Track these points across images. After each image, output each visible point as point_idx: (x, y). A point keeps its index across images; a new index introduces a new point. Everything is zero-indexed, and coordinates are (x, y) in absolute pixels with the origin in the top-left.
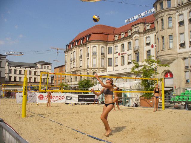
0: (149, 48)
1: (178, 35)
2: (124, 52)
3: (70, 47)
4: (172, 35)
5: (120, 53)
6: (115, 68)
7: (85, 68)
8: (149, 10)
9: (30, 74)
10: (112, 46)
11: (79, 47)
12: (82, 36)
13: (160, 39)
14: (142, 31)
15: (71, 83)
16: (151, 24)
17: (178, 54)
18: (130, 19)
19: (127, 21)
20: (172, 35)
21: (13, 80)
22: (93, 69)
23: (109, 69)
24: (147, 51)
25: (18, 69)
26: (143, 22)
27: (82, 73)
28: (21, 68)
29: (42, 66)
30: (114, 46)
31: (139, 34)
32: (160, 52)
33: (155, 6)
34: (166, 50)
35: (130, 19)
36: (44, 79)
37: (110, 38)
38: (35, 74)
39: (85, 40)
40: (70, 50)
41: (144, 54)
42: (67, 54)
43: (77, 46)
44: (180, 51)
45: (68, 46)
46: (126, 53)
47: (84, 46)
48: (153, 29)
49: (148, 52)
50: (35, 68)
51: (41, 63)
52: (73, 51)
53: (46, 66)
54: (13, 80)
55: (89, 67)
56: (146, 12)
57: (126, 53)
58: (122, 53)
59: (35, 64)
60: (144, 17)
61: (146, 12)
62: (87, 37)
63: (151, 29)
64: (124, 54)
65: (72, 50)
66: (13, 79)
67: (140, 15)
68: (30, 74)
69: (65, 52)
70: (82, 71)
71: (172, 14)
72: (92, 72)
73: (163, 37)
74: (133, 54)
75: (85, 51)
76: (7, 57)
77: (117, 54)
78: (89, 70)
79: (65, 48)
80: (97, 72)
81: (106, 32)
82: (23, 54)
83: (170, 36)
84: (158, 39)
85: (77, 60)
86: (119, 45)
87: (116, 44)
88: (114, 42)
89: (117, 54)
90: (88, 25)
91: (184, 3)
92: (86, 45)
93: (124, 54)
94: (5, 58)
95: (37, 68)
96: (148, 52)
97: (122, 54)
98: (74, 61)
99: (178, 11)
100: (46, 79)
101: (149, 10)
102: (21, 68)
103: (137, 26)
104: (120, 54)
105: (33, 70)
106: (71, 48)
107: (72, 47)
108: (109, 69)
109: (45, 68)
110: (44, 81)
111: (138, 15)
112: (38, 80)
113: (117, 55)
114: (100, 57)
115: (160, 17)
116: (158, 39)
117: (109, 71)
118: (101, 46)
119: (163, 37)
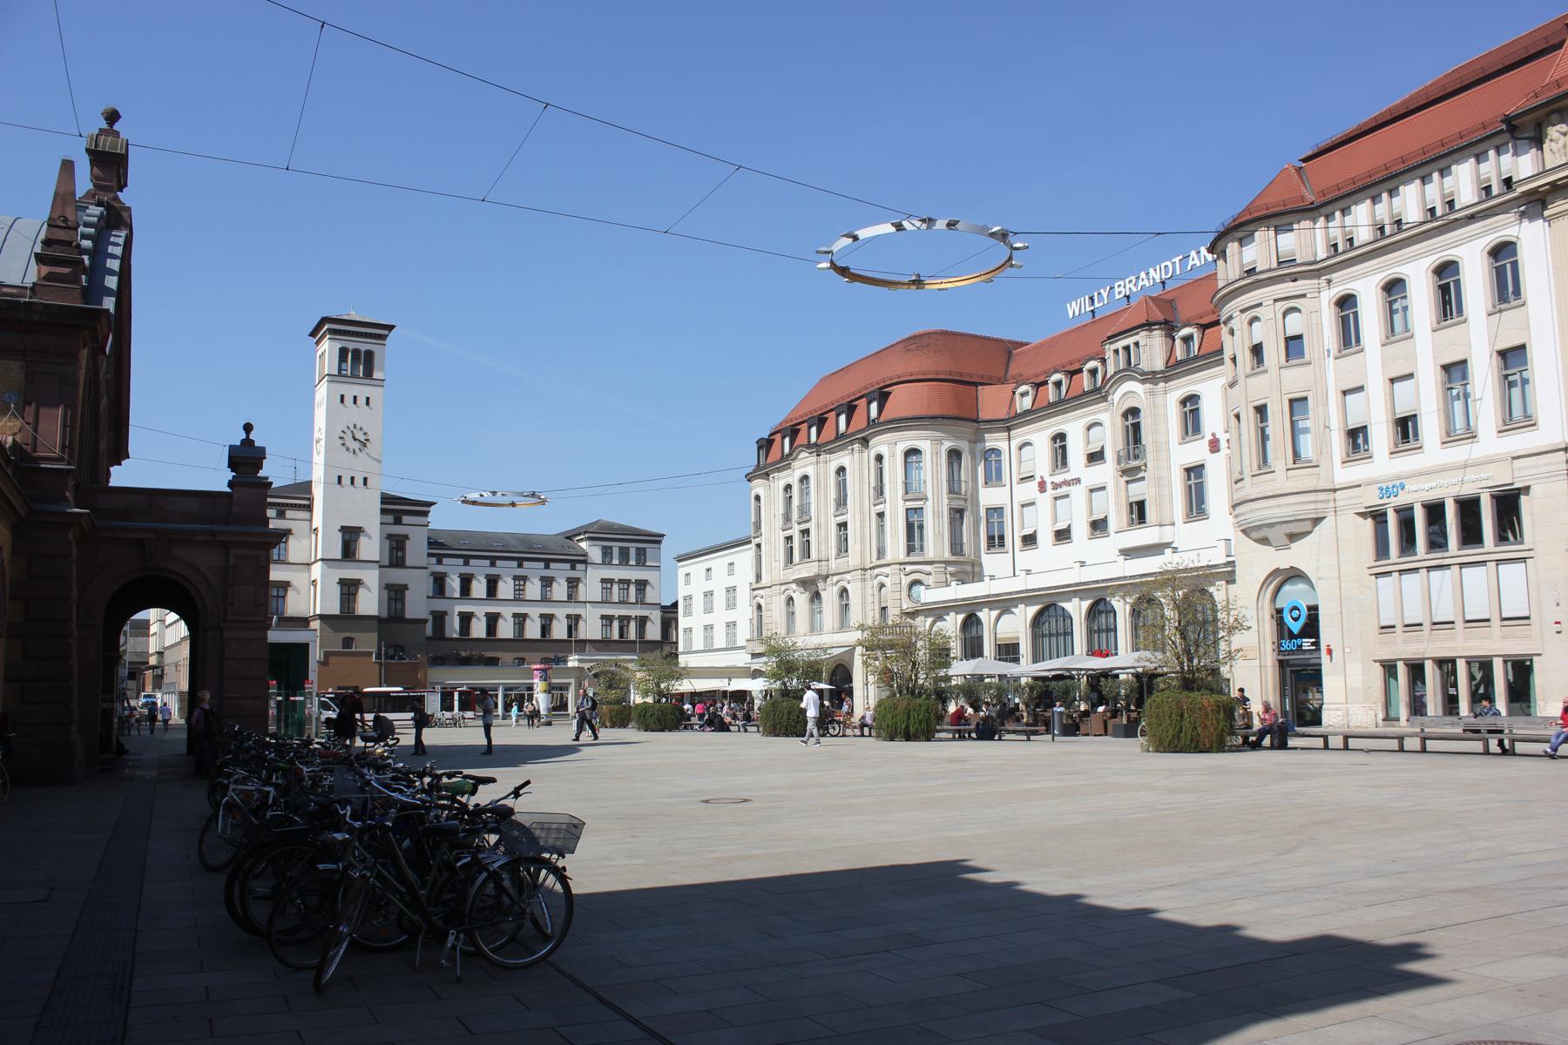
0: (1196, 451)
1: (1334, 398)
2: (1068, 476)
3: (770, 453)
4: (1305, 399)
5: (1048, 480)
6: (1026, 558)
7: (868, 565)
8: (1193, 253)
9: (519, 598)
10: (1002, 445)
11: (831, 452)
12: (842, 392)
13: (1249, 417)
14: (1159, 365)
15: (814, 641)
16: (1204, 327)
17: (1335, 490)
18: (1092, 299)
19: (1076, 308)
20: (1305, 399)
21: (538, 636)
22: (909, 568)
23: (992, 562)
24: (1188, 470)
25: (480, 570)
26: (1162, 318)
27: (849, 587)
28: (466, 563)
29: (607, 553)
30: (1015, 443)
31: (1143, 382)
32: (1248, 479)
33: (1219, 248)
34: (1280, 473)
35: (1092, 299)
36: (624, 620)
37: (991, 400)
38: (571, 597)
39: (859, 416)
40: (779, 470)
41: (1170, 485)
42: (761, 491)
43: (817, 449)
44: (1344, 475)
45: (766, 445)
46: (1078, 481)
47: (856, 446)
48: (1213, 357)
49: (1195, 472)
50: (573, 564)
51: (604, 533)
52: (798, 474)
53: (633, 547)
54: (538, 636)
55: (889, 558)
56: (1176, 260)
57: (1078, 481)
58: (1058, 479)
59: (569, 537)
60: (1168, 288)
61: (1176, 260)
62: (869, 403)
63: (1204, 357)
64: (1067, 483)
65: (788, 467)
66: (478, 630)
67: (1143, 275)
68: (709, 609)
69: (750, 478)
70: (848, 577)
71: (1304, 296)
72: (906, 581)
73: (1261, 410)
74: (1116, 485)
75: (861, 476)
76: (432, 508)
77: (1034, 485)
78: (886, 570)
79: (751, 458)
80: (930, 580)
81: (970, 369)
82: (543, 502)
83: (1297, 404)
84: (1238, 417)
85: (822, 519)
86: (1039, 436)
87: (1019, 435)
88: (1008, 424)
89: (1034, 485)
90: (870, 328)
91: (1356, 244)
92: (865, 442)
93: (1067, 483)
94: (425, 514)
95: (585, 562)
96: (1195, 472)
97: (1056, 486)
98: (804, 527)
99: (1329, 281)
100: (633, 625)
101: (1193, 253)
102: (466, 563)
103: (1130, 341)
104: (1049, 486)
105: (561, 573)
106: (784, 458)
107: (787, 450)
108: (992, 562)
109: (624, 560)
110: (621, 635)
111: (1133, 278)
112: (591, 629)
113: (1029, 491)
114: (946, 501)
115: (1242, 311)
116: (1238, 417)
117: (992, 577)
118: (947, 445)
119: (1261, 410)
